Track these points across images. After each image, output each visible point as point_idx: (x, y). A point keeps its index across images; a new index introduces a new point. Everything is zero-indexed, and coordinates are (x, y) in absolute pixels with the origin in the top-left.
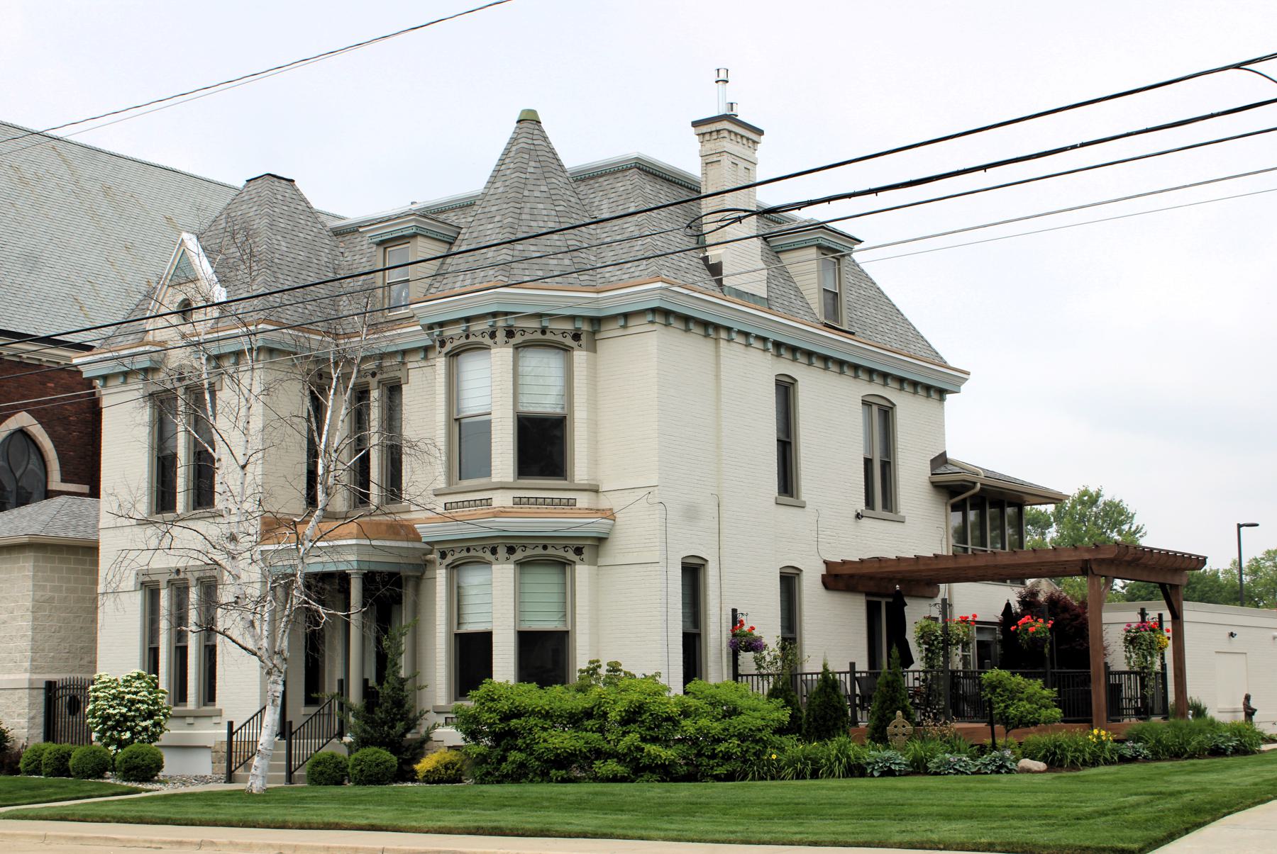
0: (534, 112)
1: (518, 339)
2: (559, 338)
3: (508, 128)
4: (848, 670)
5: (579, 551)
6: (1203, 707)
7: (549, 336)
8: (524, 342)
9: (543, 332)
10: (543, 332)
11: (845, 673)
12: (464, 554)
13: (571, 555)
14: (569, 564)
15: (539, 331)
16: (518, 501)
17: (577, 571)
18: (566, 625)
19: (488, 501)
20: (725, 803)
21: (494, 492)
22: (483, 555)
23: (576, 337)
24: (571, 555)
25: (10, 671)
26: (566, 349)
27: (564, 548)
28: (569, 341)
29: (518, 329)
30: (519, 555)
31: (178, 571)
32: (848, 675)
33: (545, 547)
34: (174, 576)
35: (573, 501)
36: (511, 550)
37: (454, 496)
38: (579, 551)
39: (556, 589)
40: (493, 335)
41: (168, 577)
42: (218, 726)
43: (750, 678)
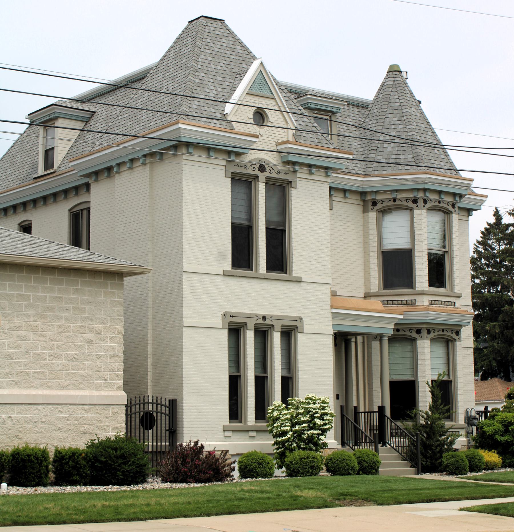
0: (397, 66)
1: (379, 206)
2: (404, 203)
3: (381, 75)
4: (377, 410)
5: (419, 332)
6: (218, 454)
7: (398, 202)
8: (432, 207)
9: (395, 200)
10: (395, 200)
11: (376, 412)
12: (441, 333)
13: (414, 335)
14: (451, 341)
15: (392, 200)
16: (431, 302)
17: (418, 344)
18: (449, 377)
19: (413, 302)
20: (53, 514)
21: (417, 296)
22: (410, 334)
23: (415, 201)
24: (414, 335)
25: (98, 388)
26: (411, 210)
27: (410, 330)
28: (410, 204)
29: (379, 201)
30: (432, 335)
31: (264, 318)
32: (377, 413)
33: (443, 331)
34: (261, 321)
35: (414, 301)
36: (429, 332)
37: (439, 297)
38: (419, 332)
39: (409, 355)
40: (415, 201)
41: (254, 321)
42: (228, 439)
43: (372, 414)
